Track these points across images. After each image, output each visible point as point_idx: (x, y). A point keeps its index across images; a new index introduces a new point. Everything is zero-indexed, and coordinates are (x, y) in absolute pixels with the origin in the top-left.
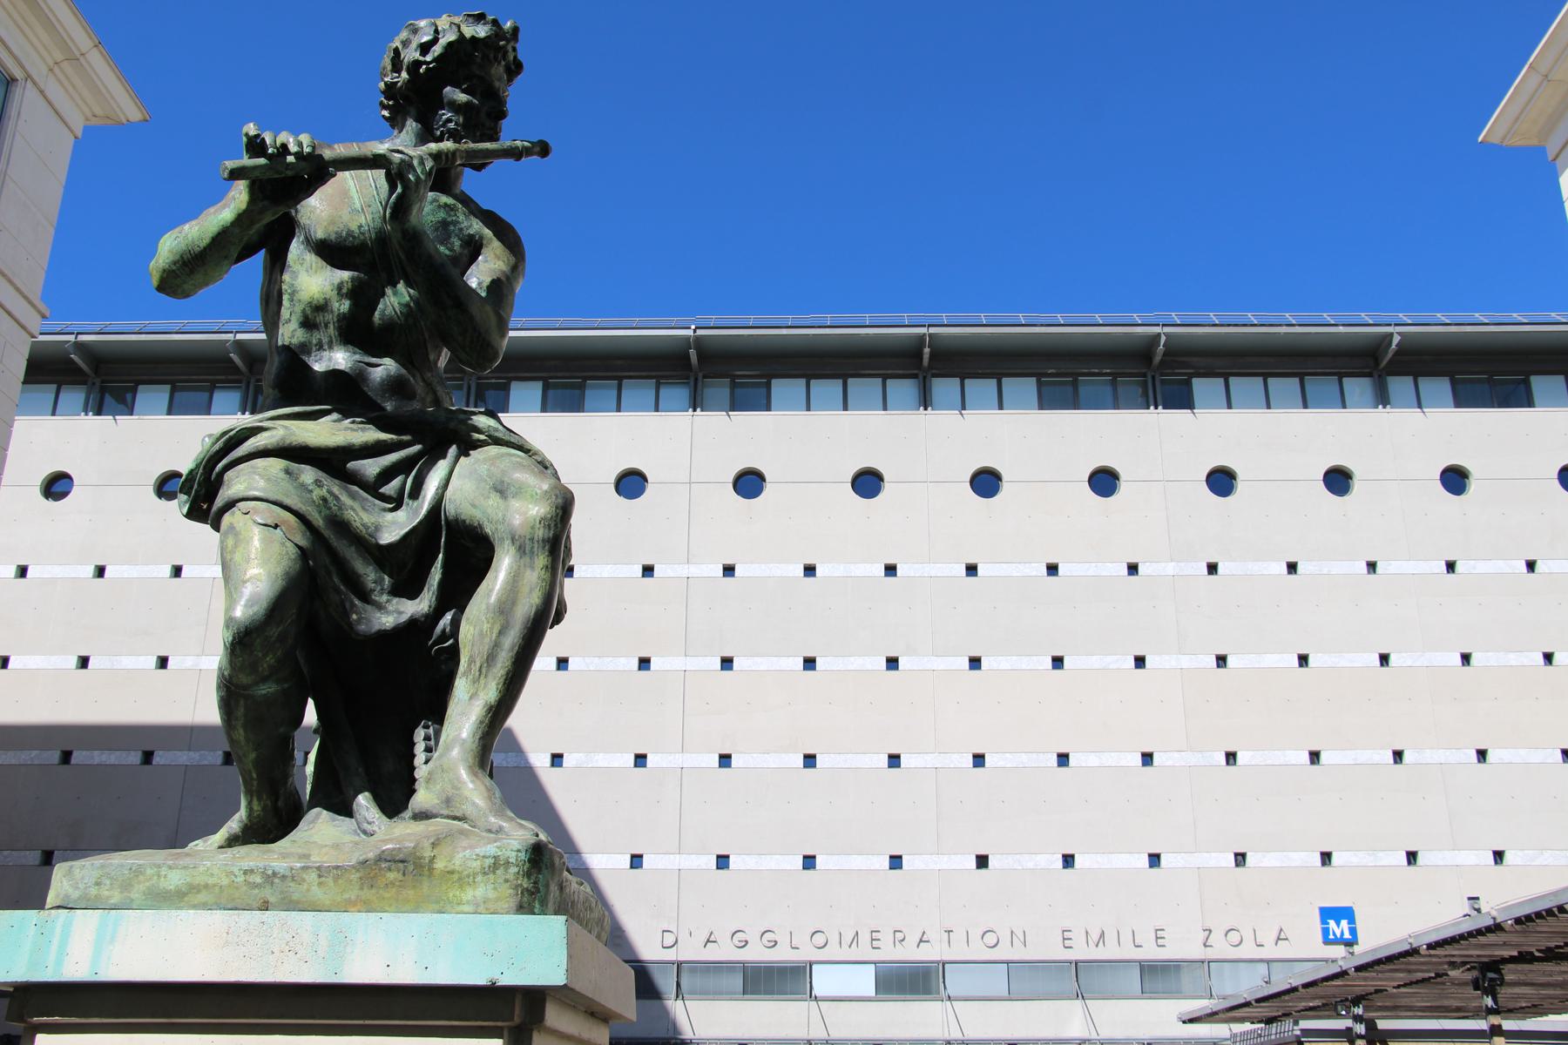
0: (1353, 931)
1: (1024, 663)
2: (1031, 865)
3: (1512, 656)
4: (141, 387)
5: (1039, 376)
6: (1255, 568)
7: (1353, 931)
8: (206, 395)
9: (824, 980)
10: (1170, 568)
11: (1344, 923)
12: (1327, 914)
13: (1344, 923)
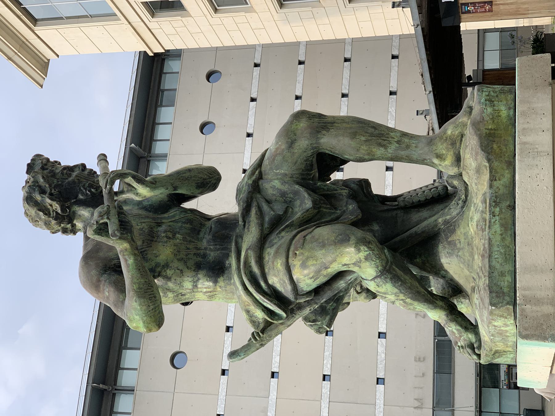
2: (383, 356)
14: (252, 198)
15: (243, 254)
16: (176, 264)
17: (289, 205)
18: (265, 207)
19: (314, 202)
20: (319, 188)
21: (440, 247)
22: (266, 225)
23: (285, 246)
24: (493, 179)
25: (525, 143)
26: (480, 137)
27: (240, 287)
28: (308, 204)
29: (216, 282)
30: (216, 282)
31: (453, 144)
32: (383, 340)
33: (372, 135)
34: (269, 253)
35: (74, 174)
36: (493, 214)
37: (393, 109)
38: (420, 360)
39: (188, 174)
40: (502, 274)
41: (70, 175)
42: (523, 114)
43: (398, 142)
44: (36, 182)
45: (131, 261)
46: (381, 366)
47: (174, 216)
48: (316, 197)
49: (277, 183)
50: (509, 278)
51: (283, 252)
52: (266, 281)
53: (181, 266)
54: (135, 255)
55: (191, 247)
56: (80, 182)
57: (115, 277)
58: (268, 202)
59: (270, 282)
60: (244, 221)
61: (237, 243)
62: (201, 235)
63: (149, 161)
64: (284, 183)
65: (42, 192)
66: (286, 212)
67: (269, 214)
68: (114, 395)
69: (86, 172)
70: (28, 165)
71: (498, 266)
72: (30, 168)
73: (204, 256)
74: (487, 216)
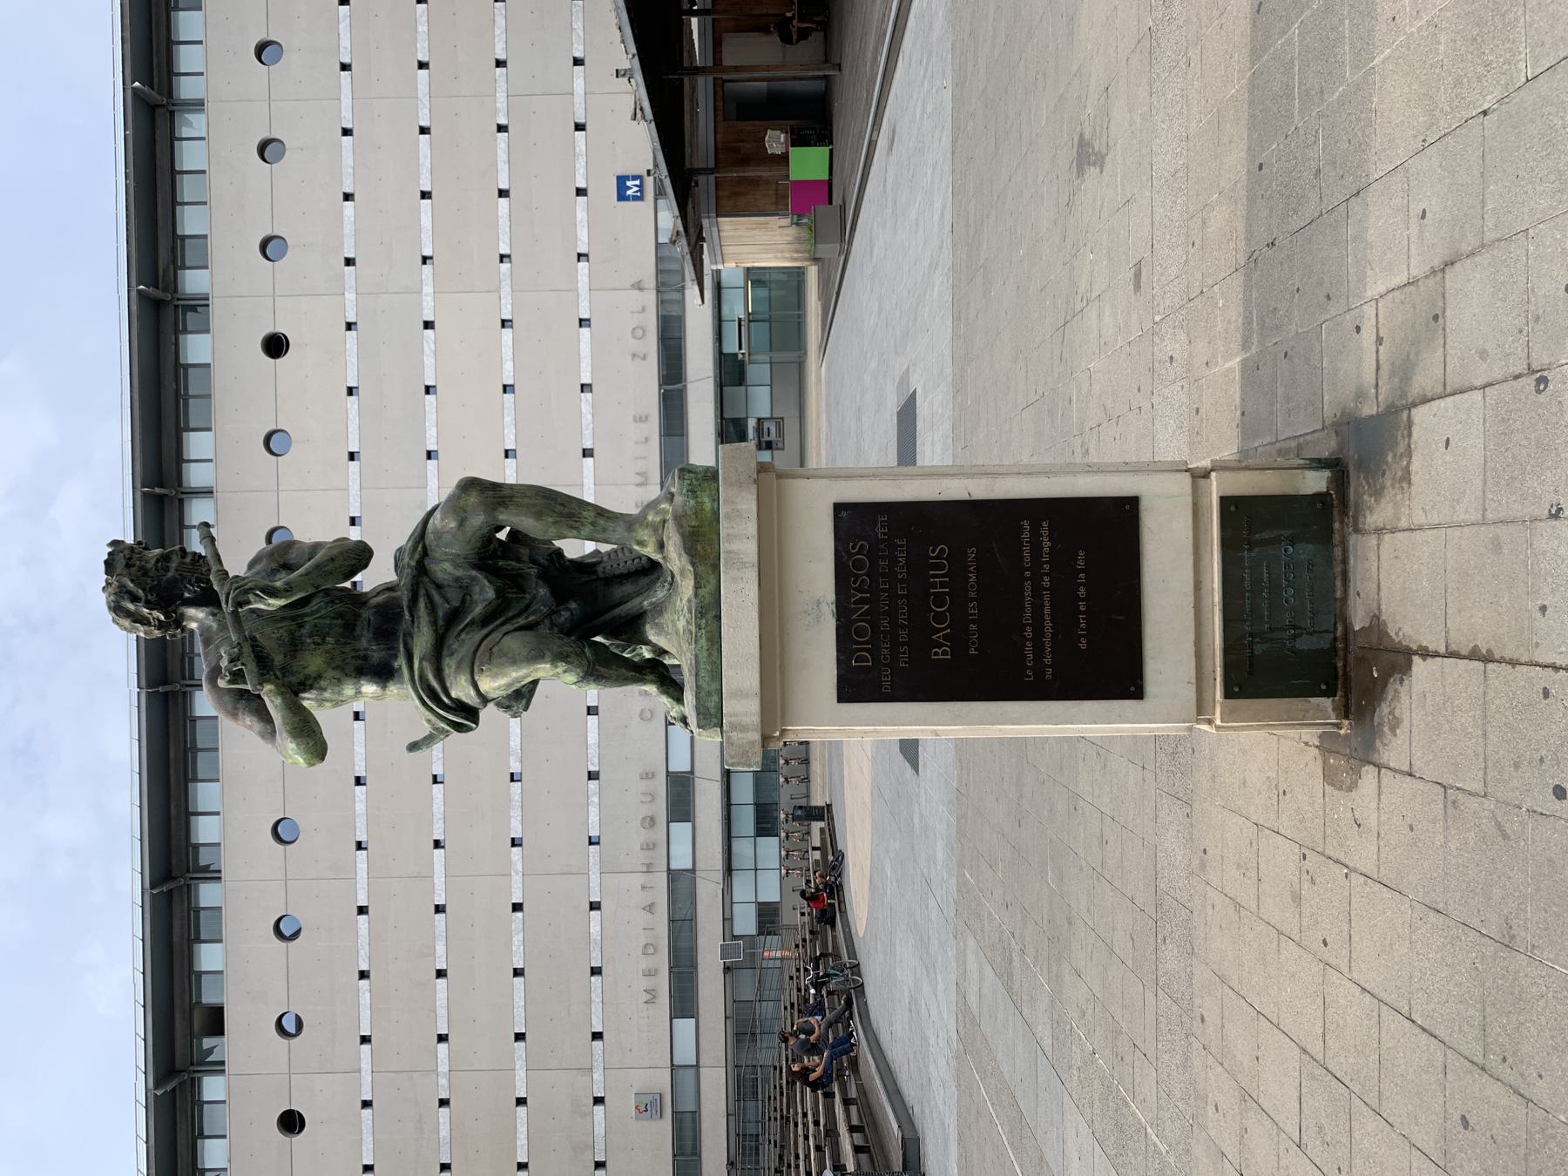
0: (635, 178)
1: (431, 416)
2: (590, 417)
3: (420, 29)
4: (193, 841)
5: (177, 332)
6: (348, 228)
7: (635, 178)
8: (191, 371)
9: (681, 861)
10: (350, 296)
11: (629, 183)
12: (622, 197)
13: (629, 183)
14: (418, 584)
15: (416, 665)
16: (330, 674)
17: (466, 590)
18: (436, 597)
19: (497, 591)
20: (501, 568)
21: (648, 627)
22: (441, 623)
23: (468, 660)
24: (697, 586)
25: (730, 552)
26: (683, 535)
27: (417, 702)
28: (490, 594)
29: (384, 687)
30: (384, 687)
31: (655, 530)
32: (589, 395)
33: (561, 515)
34: (449, 665)
35: (173, 565)
36: (699, 627)
37: (580, 24)
38: (641, 419)
39: (331, 566)
40: (709, 694)
41: (167, 569)
42: (727, 516)
43: (593, 524)
44: (122, 587)
45: (278, 701)
46: (587, 433)
47: (318, 611)
48: (499, 583)
49: (447, 566)
50: (715, 698)
51: (466, 666)
52: (448, 696)
53: (337, 674)
54: (282, 694)
55: (347, 649)
56: (183, 577)
57: (255, 704)
58: (439, 587)
59: (453, 694)
60: (412, 615)
61: (406, 644)
62: (358, 629)
63: (172, 113)
64: (457, 566)
65: (134, 599)
66: (463, 601)
67: (443, 608)
68: (181, 501)
69: (188, 560)
70: (106, 562)
71: (705, 685)
72: (109, 565)
73: (366, 658)
74: (693, 628)
